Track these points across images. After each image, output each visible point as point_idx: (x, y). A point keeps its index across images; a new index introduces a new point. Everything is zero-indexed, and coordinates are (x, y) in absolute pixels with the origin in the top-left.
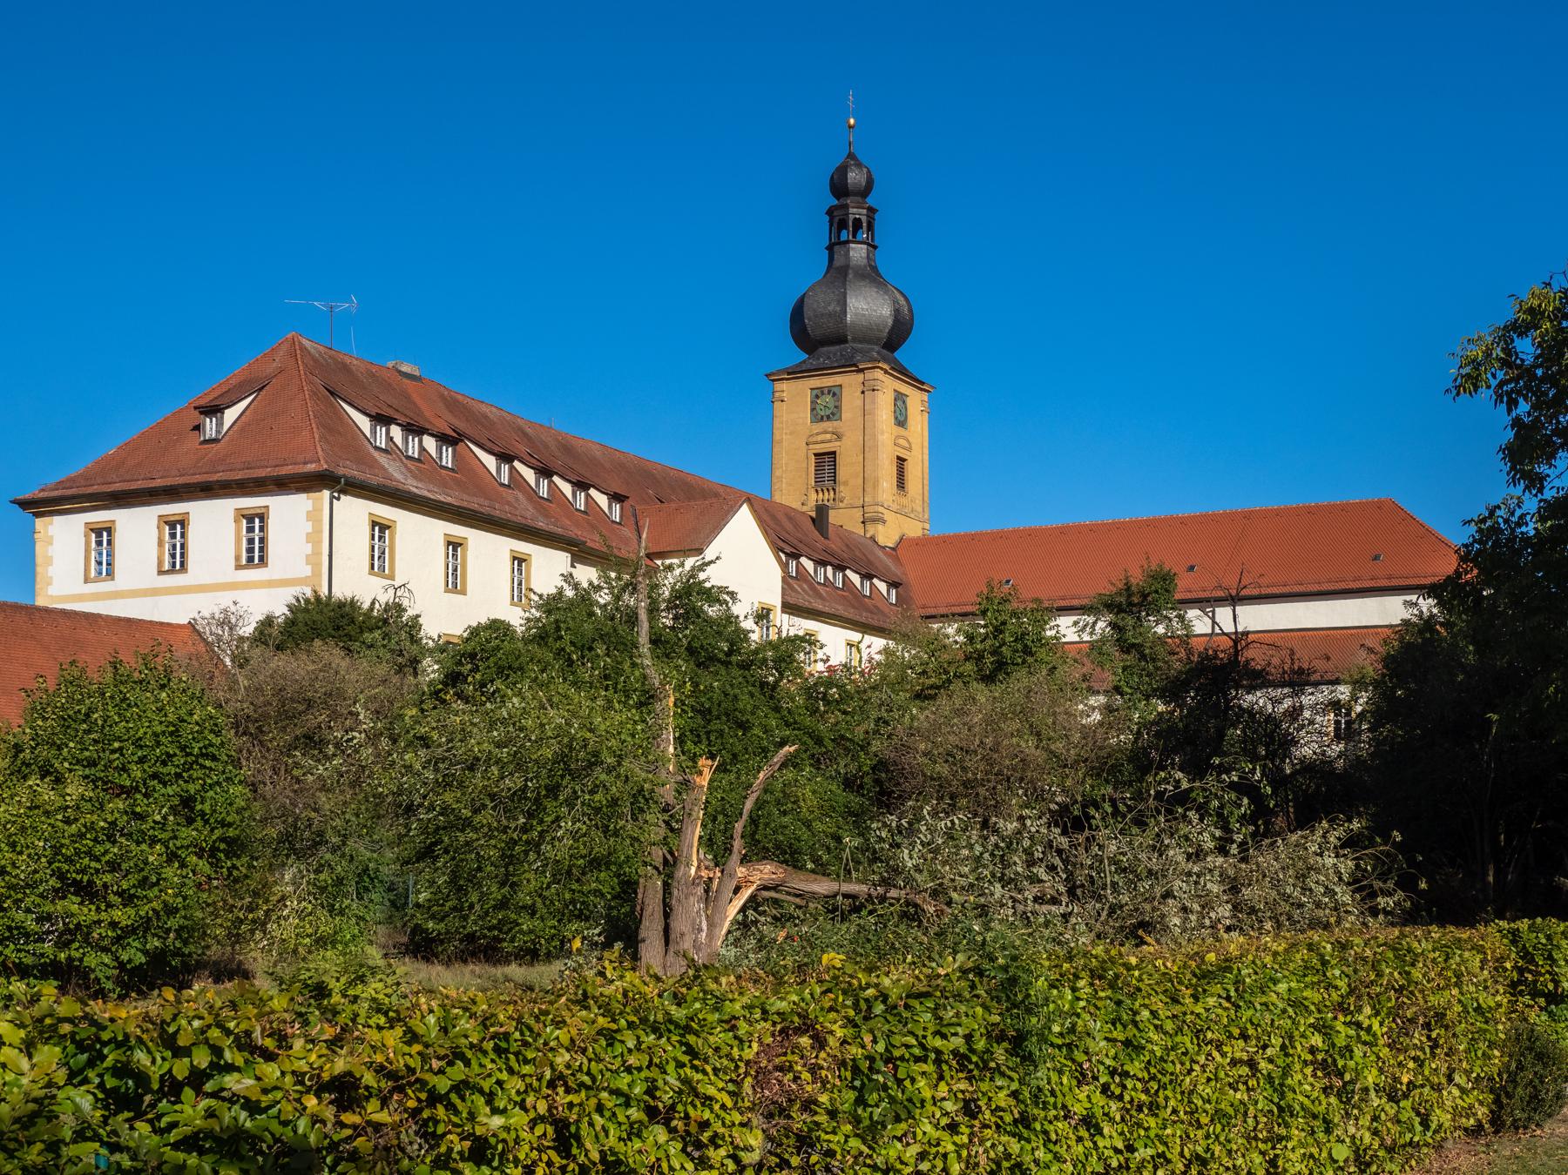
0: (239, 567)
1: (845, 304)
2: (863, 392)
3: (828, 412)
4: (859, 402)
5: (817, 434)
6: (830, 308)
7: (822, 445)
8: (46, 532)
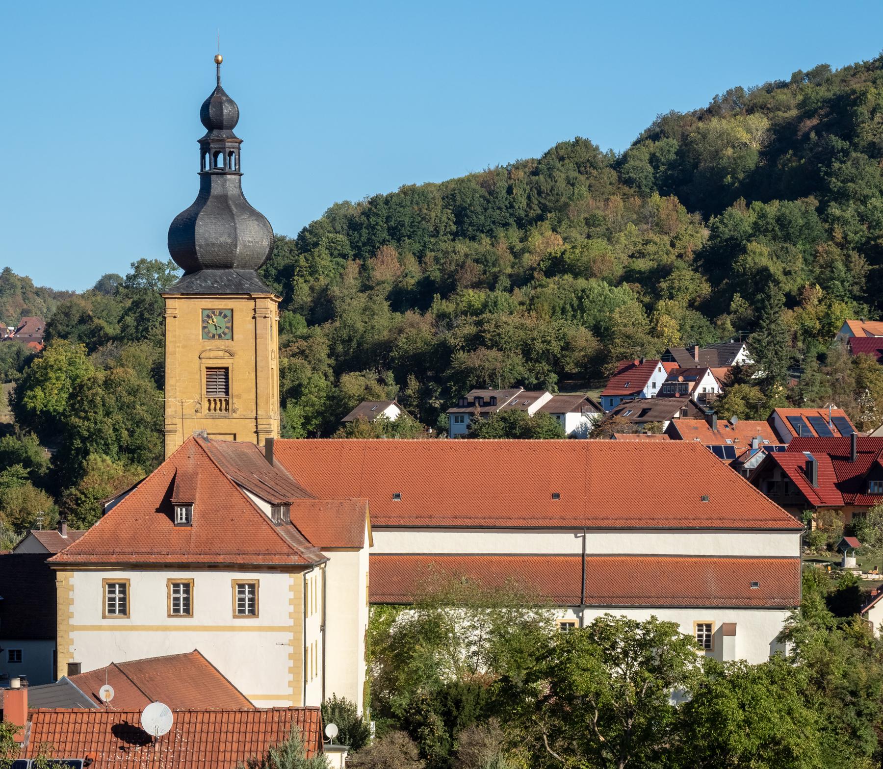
1: (236, 237)
2: (254, 318)
3: (220, 331)
5: (210, 350)
6: (222, 240)
7: (215, 361)
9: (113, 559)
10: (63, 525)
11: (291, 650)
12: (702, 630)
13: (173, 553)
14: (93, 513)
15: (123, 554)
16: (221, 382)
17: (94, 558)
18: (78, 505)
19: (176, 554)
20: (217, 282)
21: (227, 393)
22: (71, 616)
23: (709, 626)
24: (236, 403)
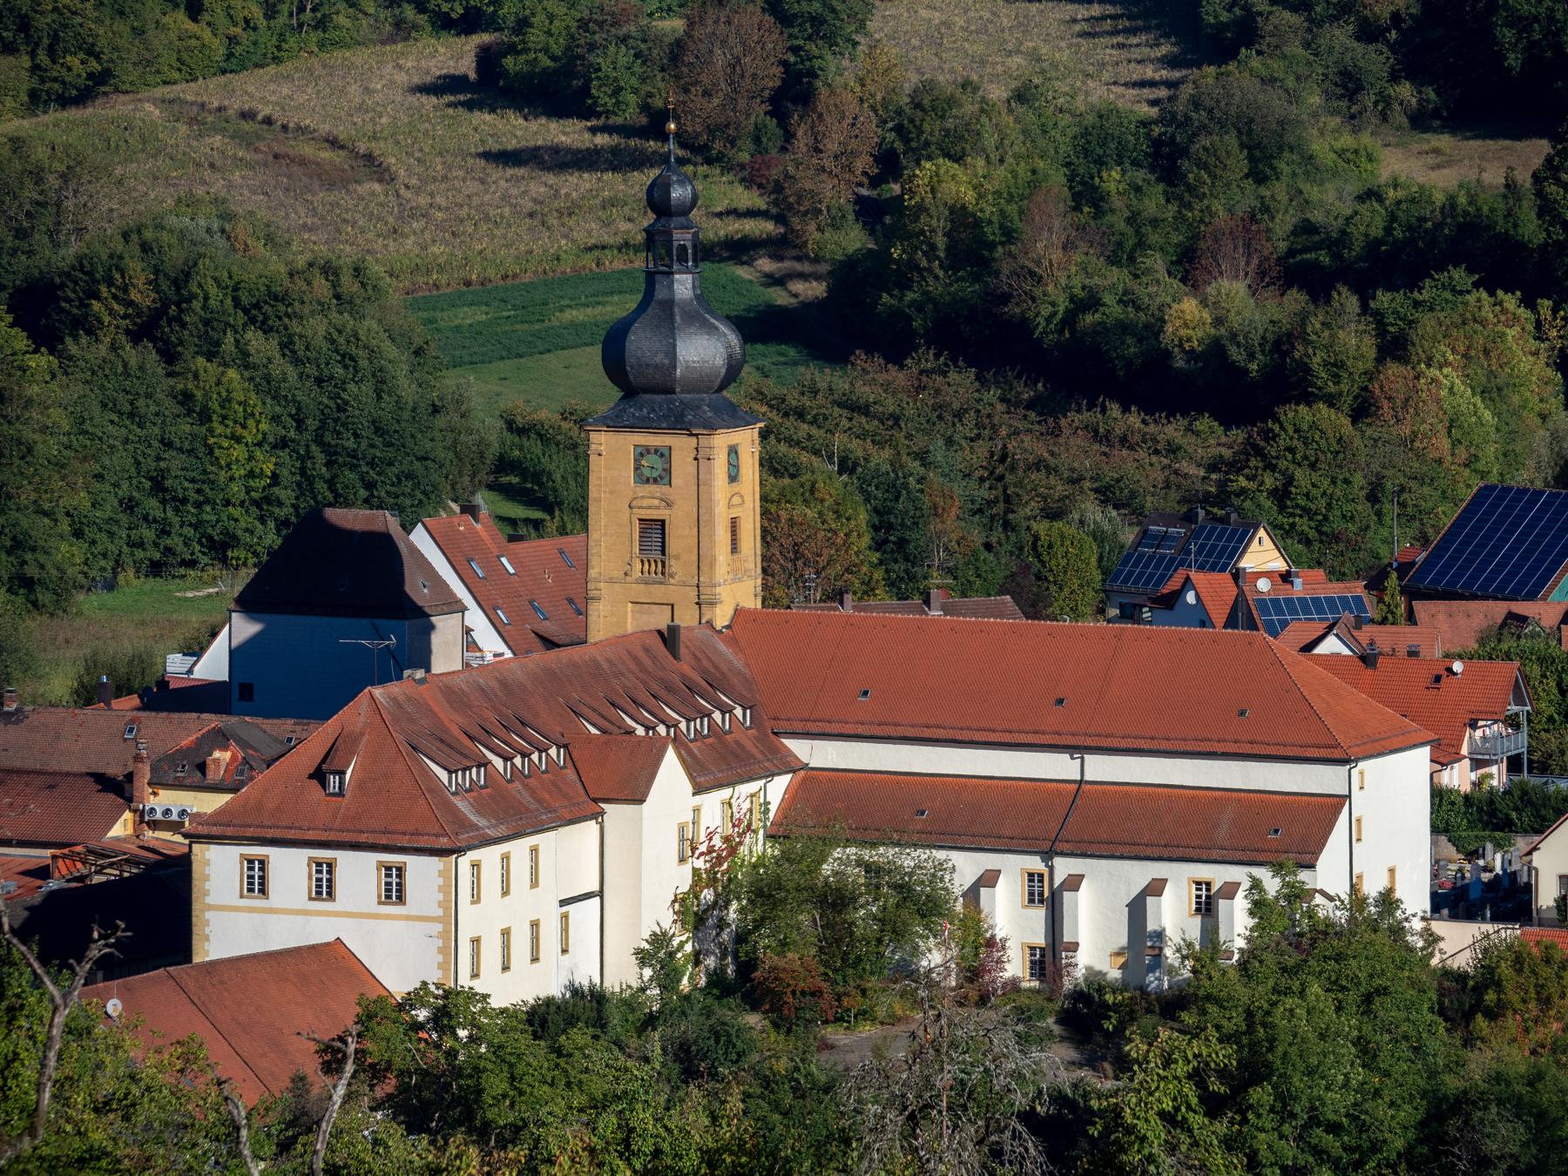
0: (380, 903)
2: (696, 459)
3: (655, 474)
4: (693, 470)
5: (643, 497)
7: (649, 511)
8: (203, 855)
9: (250, 832)
10: (845, 596)
11: (440, 943)
12: (1200, 890)
13: (314, 829)
14: (1290, 456)
15: (263, 827)
16: (657, 537)
17: (229, 831)
18: (1267, 440)
19: (317, 829)
20: (654, 410)
21: (664, 554)
22: (207, 893)
23: (1208, 884)
24: (674, 566)
